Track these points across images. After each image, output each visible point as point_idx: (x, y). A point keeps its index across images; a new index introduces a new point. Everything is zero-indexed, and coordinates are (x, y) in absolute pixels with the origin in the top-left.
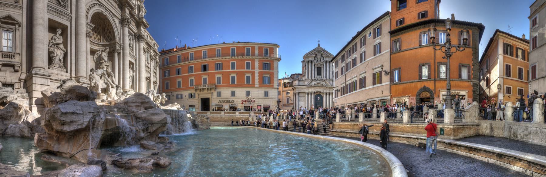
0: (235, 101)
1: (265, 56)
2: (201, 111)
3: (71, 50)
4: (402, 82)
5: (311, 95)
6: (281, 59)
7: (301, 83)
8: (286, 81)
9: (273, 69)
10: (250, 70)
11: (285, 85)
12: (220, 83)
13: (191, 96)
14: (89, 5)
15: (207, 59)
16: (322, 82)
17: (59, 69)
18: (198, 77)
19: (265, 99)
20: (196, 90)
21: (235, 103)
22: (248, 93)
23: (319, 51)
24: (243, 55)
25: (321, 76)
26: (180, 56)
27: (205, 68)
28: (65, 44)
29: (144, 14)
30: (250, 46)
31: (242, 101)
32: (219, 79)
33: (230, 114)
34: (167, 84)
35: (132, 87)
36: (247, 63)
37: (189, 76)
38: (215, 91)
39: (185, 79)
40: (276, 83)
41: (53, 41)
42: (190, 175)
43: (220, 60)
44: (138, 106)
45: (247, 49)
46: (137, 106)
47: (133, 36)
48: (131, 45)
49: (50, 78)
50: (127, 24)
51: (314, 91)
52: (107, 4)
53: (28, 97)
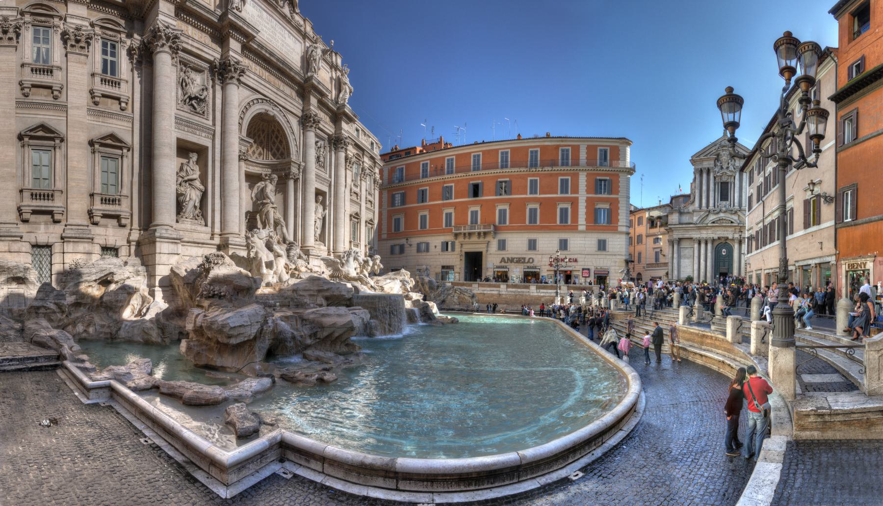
0: (536, 260)
1: (601, 165)
2: (466, 280)
4: (859, 221)
5: (706, 244)
6: (635, 171)
7: (686, 219)
8: (655, 214)
9: (617, 193)
10: (569, 195)
11: (652, 222)
12: (505, 223)
13: (445, 246)
14: (244, 104)
15: (482, 173)
16: (730, 216)
17: (194, 221)
18: (461, 209)
19: (600, 257)
20: (456, 235)
21: (535, 263)
22: (564, 245)
23: (724, 146)
24: (554, 164)
25: (728, 203)
26: (427, 164)
27: (476, 190)
28: (204, 179)
29: (348, 96)
30: (569, 146)
32: (503, 213)
33: (519, 290)
34: (398, 221)
35: (322, 238)
36: (562, 180)
37: (444, 205)
38: (494, 238)
39: (436, 211)
40: (623, 218)
41: (183, 174)
42: (819, 503)
43: (507, 174)
44: (314, 295)
45: (563, 151)
46: (311, 295)
47: (326, 141)
48: (322, 159)
50: (312, 126)
51: (712, 236)
53: (146, 274)
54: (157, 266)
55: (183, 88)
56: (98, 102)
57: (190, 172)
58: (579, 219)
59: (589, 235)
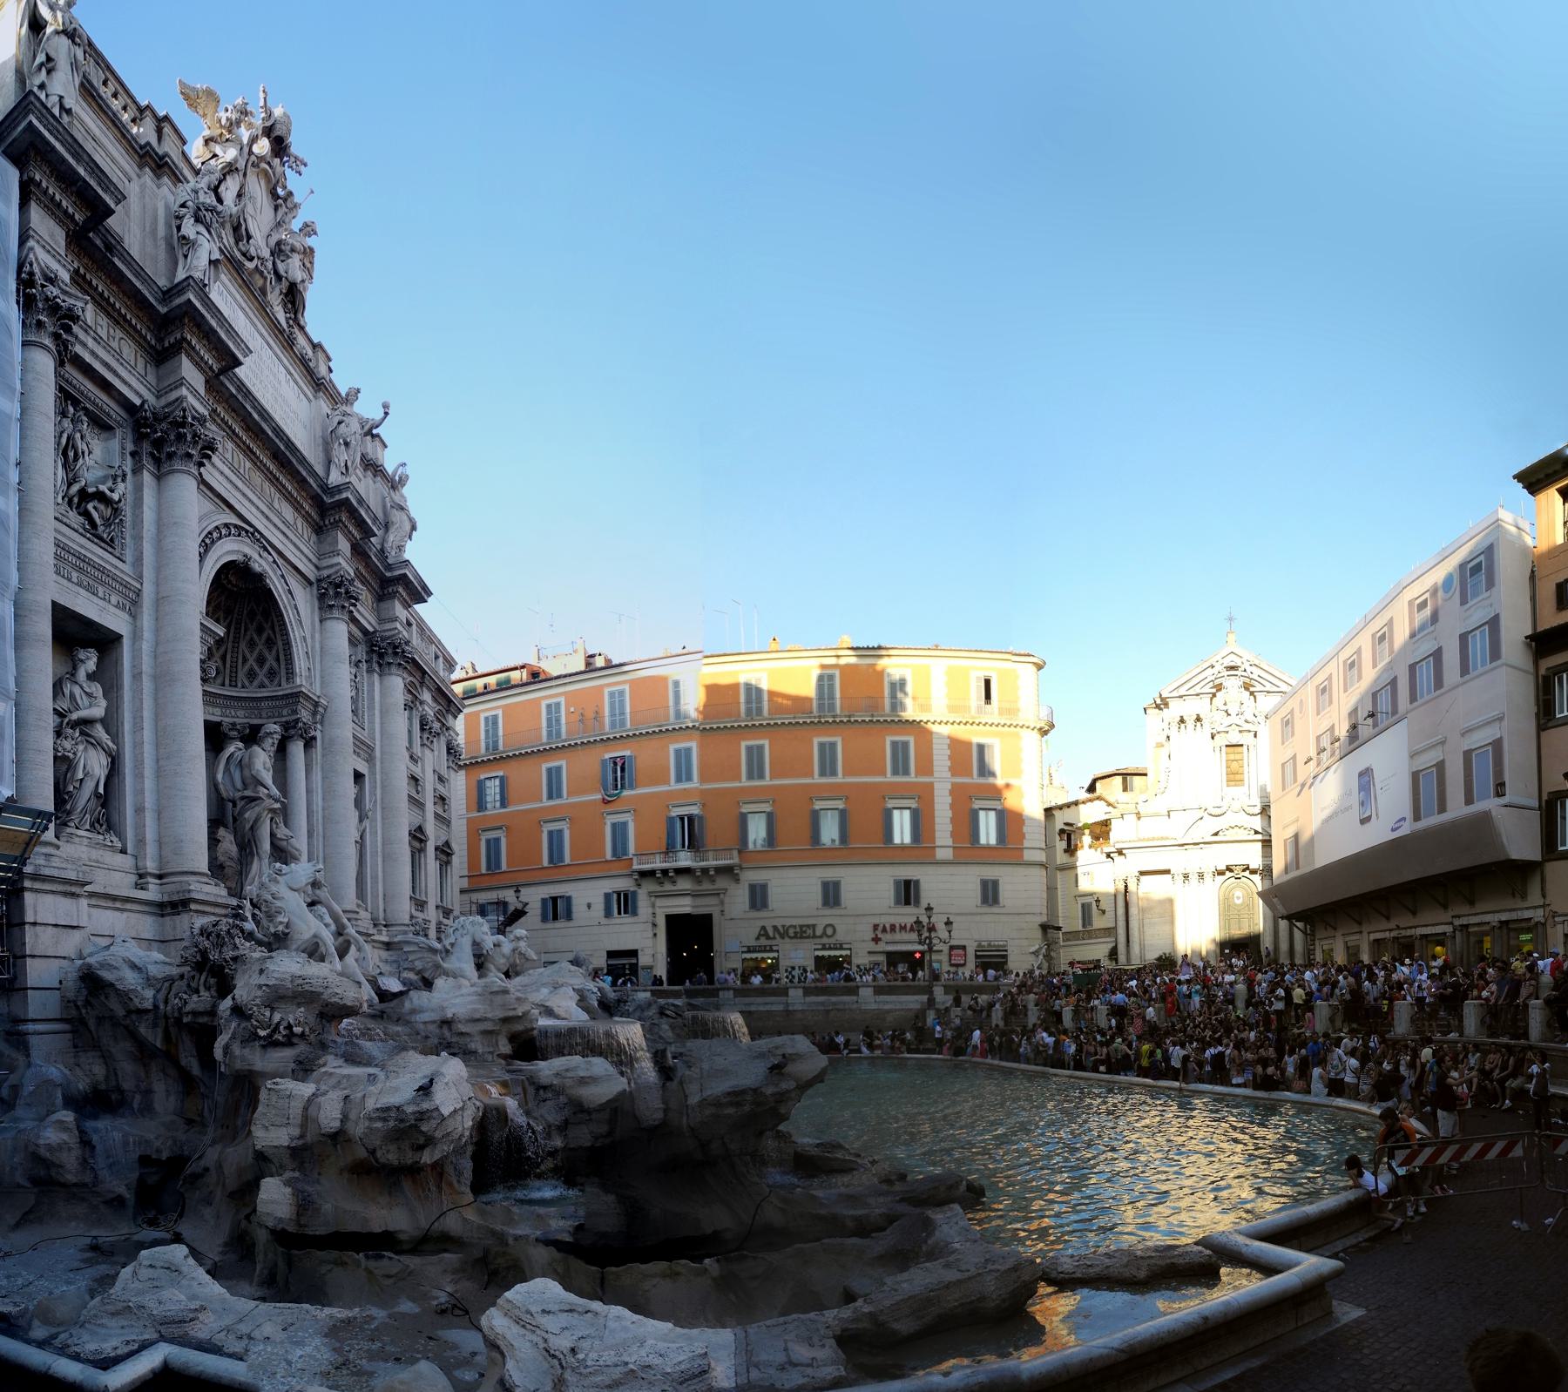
3: (138, 745)
19: (987, 918)
21: (841, 936)
26: (558, 705)
31: (876, 927)
33: (834, 999)
34: (493, 846)
49: (87, 888)
52: (264, 521)
54: (29, 961)
55: (65, 466)
56: (306, 225)
57: (82, 700)
58: (938, 834)
59: (962, 869)
